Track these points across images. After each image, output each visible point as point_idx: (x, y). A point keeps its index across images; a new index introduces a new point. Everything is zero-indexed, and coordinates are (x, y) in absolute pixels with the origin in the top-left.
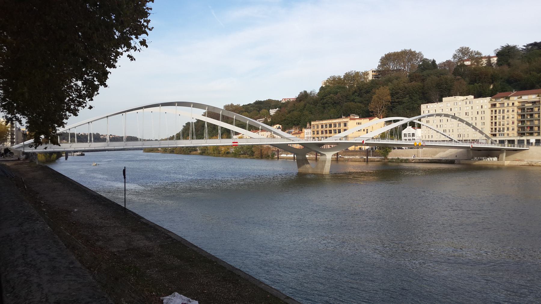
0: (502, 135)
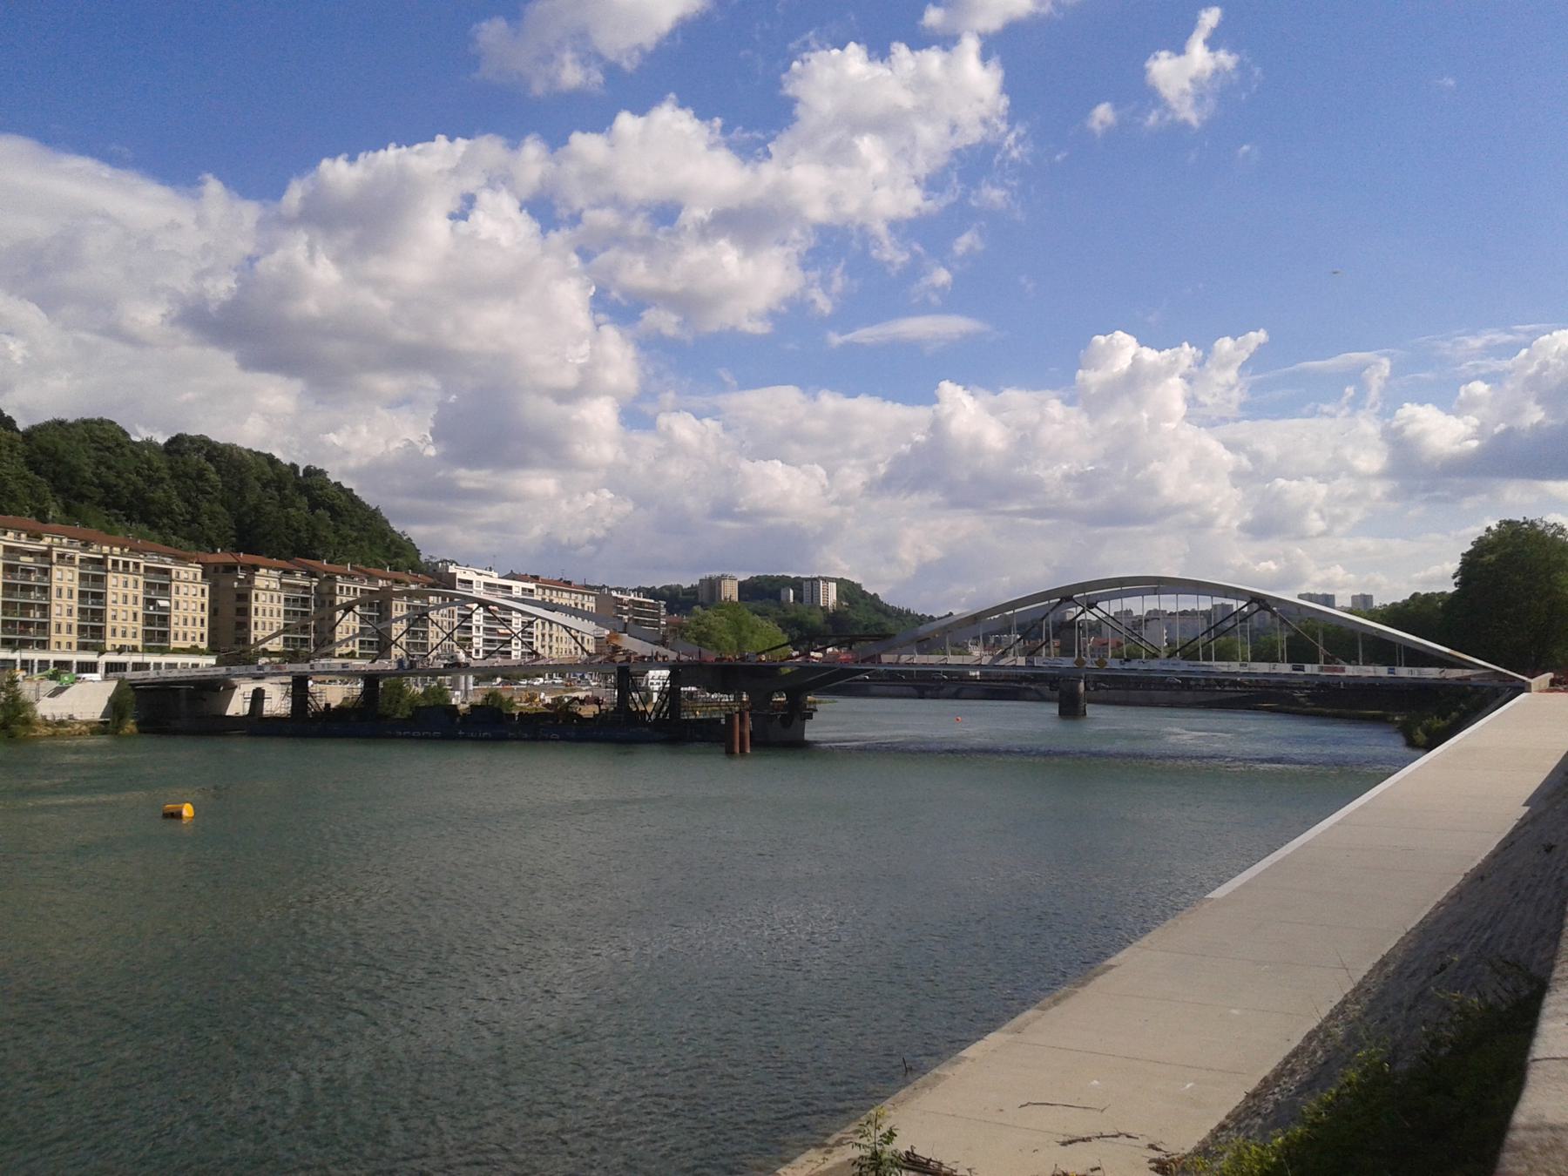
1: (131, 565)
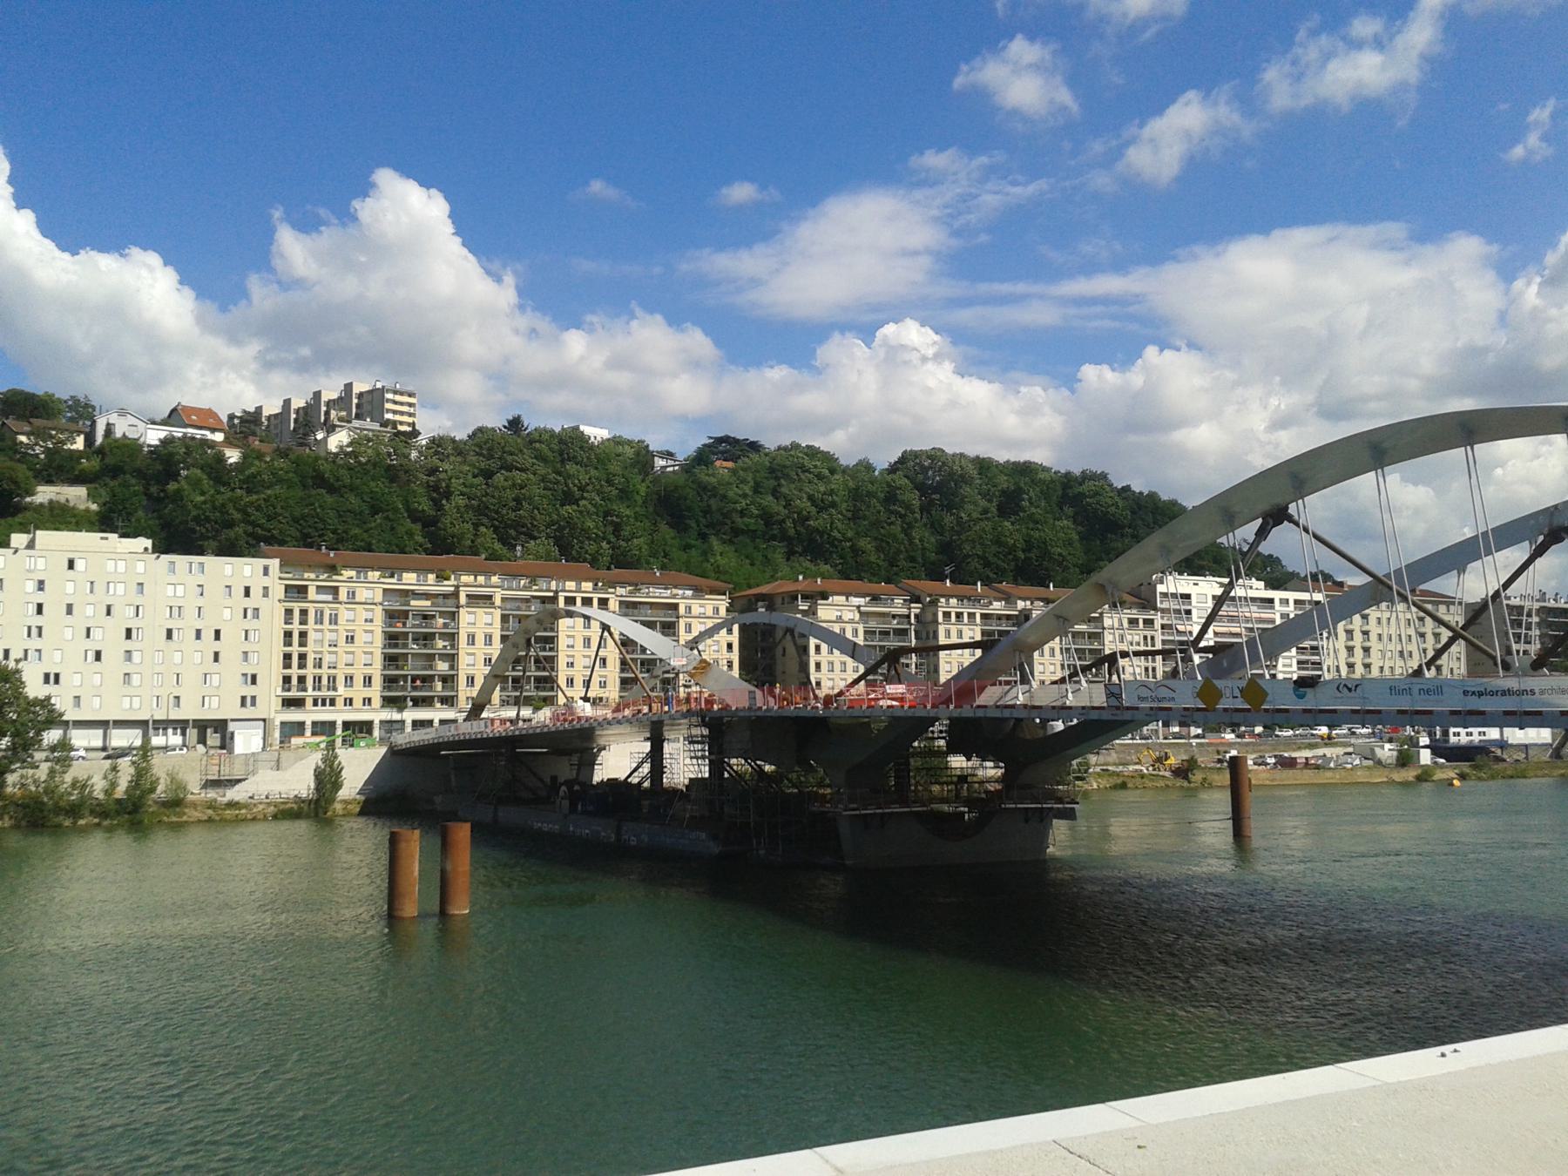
0: (324, 704)
1: (966, 615)
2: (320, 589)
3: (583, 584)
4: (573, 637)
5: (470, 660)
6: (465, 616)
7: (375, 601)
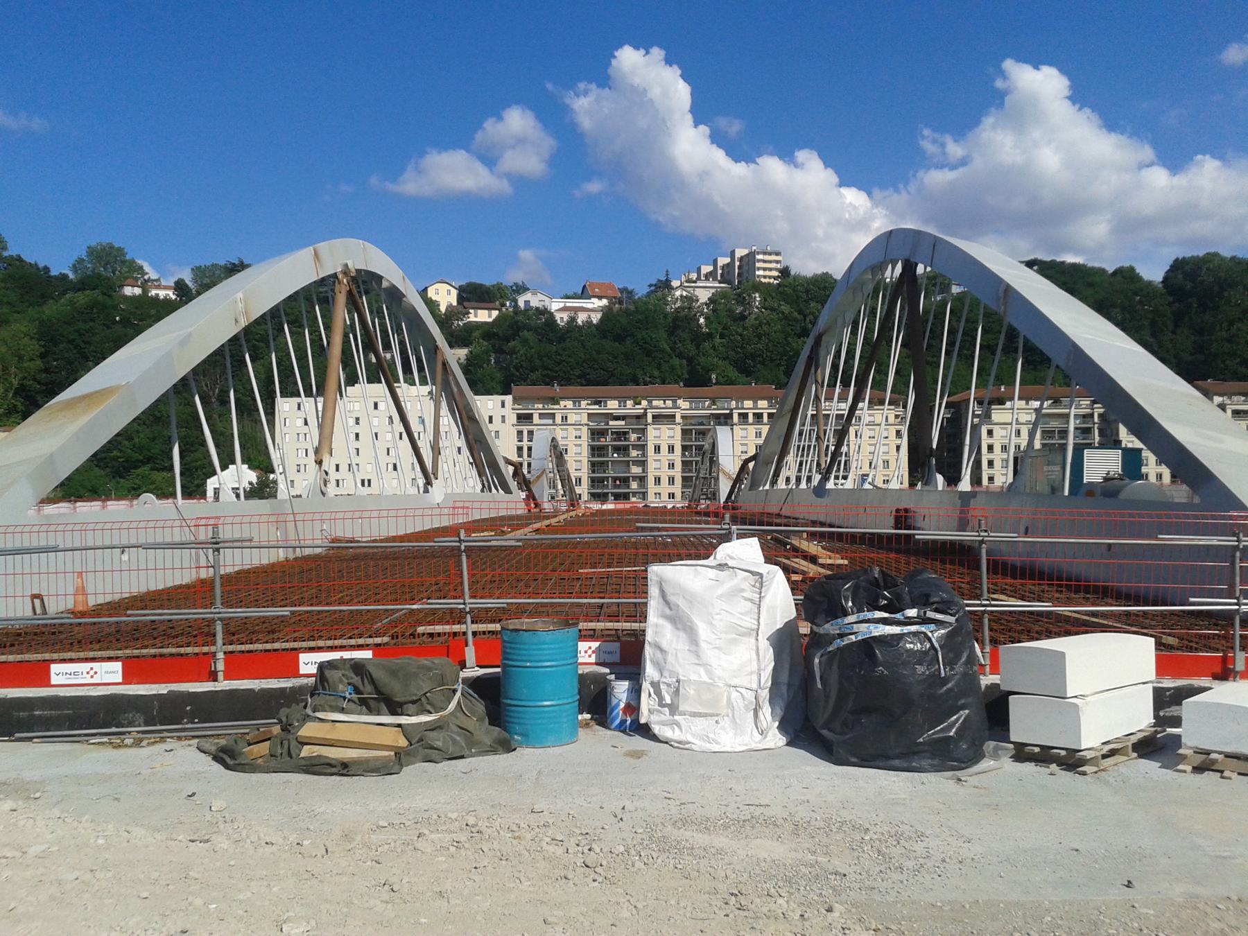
2: (541, 416)
3: (759, 402)
4: (746, 444)
5: (657, 465)
6: (652, 432)
7: (582, 423)
